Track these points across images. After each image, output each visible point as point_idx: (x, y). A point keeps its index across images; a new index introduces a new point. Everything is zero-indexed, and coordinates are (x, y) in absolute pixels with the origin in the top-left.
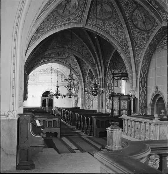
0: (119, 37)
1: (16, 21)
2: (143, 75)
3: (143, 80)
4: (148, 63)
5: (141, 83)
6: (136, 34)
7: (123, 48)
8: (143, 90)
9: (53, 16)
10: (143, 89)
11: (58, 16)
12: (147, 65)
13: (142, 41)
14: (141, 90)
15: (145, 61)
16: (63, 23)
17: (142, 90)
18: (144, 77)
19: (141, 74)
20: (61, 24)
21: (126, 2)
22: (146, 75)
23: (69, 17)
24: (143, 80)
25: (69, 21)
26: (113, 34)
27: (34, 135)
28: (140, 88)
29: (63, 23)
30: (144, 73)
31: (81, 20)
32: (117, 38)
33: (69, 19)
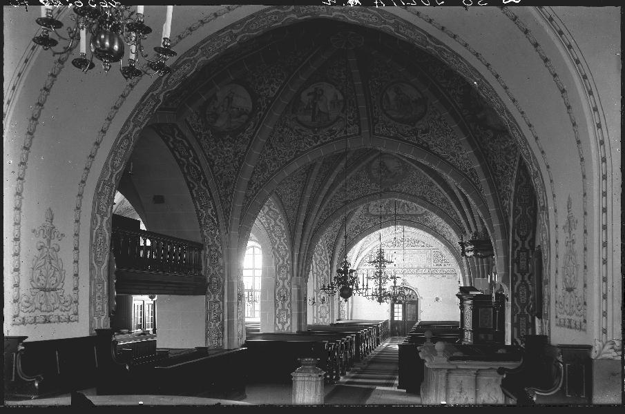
0: (453, 154)
1: (569, 36)
2: (520, 242)
3: (523, 255)
4: (532, 212)
5: (518, 264)
6: (490, 143)
7: (471, 180)
8: (523, 280)
9: (291, 129)
10: (523, 278)
11: (304, 128)
12: (529, 216)
13: (506, 158)
14: (518, 282)
15: (520, 208)
16: (319, 143)
17: (522, 281)
18: (525, 248)
19: (514, 241)
20: (315, 144)
21: (444, 71)
22: (529, 243)
23: (331, 127)
24: (523, 255)
25: (333, 136)
26: (439, 151)
27: (552, 391)
28: (513, 275)
29: (319, 143)
30: (523, 238)
31: (99, 206)
32: (451, 157)
33: (332, 132)
